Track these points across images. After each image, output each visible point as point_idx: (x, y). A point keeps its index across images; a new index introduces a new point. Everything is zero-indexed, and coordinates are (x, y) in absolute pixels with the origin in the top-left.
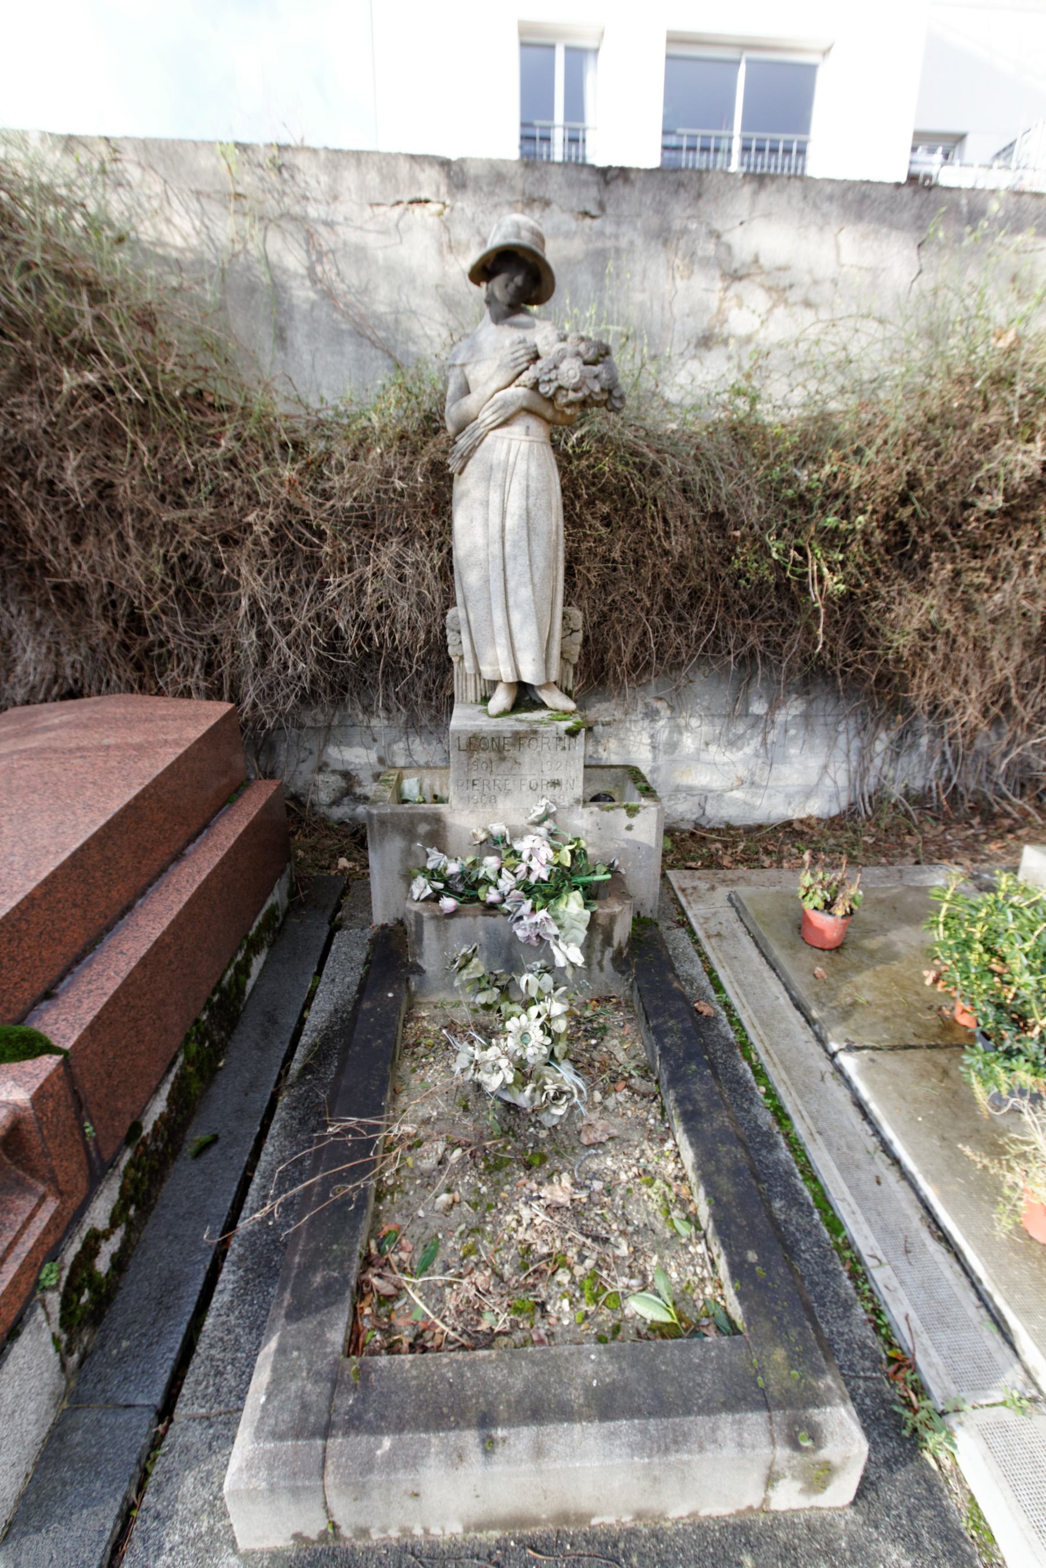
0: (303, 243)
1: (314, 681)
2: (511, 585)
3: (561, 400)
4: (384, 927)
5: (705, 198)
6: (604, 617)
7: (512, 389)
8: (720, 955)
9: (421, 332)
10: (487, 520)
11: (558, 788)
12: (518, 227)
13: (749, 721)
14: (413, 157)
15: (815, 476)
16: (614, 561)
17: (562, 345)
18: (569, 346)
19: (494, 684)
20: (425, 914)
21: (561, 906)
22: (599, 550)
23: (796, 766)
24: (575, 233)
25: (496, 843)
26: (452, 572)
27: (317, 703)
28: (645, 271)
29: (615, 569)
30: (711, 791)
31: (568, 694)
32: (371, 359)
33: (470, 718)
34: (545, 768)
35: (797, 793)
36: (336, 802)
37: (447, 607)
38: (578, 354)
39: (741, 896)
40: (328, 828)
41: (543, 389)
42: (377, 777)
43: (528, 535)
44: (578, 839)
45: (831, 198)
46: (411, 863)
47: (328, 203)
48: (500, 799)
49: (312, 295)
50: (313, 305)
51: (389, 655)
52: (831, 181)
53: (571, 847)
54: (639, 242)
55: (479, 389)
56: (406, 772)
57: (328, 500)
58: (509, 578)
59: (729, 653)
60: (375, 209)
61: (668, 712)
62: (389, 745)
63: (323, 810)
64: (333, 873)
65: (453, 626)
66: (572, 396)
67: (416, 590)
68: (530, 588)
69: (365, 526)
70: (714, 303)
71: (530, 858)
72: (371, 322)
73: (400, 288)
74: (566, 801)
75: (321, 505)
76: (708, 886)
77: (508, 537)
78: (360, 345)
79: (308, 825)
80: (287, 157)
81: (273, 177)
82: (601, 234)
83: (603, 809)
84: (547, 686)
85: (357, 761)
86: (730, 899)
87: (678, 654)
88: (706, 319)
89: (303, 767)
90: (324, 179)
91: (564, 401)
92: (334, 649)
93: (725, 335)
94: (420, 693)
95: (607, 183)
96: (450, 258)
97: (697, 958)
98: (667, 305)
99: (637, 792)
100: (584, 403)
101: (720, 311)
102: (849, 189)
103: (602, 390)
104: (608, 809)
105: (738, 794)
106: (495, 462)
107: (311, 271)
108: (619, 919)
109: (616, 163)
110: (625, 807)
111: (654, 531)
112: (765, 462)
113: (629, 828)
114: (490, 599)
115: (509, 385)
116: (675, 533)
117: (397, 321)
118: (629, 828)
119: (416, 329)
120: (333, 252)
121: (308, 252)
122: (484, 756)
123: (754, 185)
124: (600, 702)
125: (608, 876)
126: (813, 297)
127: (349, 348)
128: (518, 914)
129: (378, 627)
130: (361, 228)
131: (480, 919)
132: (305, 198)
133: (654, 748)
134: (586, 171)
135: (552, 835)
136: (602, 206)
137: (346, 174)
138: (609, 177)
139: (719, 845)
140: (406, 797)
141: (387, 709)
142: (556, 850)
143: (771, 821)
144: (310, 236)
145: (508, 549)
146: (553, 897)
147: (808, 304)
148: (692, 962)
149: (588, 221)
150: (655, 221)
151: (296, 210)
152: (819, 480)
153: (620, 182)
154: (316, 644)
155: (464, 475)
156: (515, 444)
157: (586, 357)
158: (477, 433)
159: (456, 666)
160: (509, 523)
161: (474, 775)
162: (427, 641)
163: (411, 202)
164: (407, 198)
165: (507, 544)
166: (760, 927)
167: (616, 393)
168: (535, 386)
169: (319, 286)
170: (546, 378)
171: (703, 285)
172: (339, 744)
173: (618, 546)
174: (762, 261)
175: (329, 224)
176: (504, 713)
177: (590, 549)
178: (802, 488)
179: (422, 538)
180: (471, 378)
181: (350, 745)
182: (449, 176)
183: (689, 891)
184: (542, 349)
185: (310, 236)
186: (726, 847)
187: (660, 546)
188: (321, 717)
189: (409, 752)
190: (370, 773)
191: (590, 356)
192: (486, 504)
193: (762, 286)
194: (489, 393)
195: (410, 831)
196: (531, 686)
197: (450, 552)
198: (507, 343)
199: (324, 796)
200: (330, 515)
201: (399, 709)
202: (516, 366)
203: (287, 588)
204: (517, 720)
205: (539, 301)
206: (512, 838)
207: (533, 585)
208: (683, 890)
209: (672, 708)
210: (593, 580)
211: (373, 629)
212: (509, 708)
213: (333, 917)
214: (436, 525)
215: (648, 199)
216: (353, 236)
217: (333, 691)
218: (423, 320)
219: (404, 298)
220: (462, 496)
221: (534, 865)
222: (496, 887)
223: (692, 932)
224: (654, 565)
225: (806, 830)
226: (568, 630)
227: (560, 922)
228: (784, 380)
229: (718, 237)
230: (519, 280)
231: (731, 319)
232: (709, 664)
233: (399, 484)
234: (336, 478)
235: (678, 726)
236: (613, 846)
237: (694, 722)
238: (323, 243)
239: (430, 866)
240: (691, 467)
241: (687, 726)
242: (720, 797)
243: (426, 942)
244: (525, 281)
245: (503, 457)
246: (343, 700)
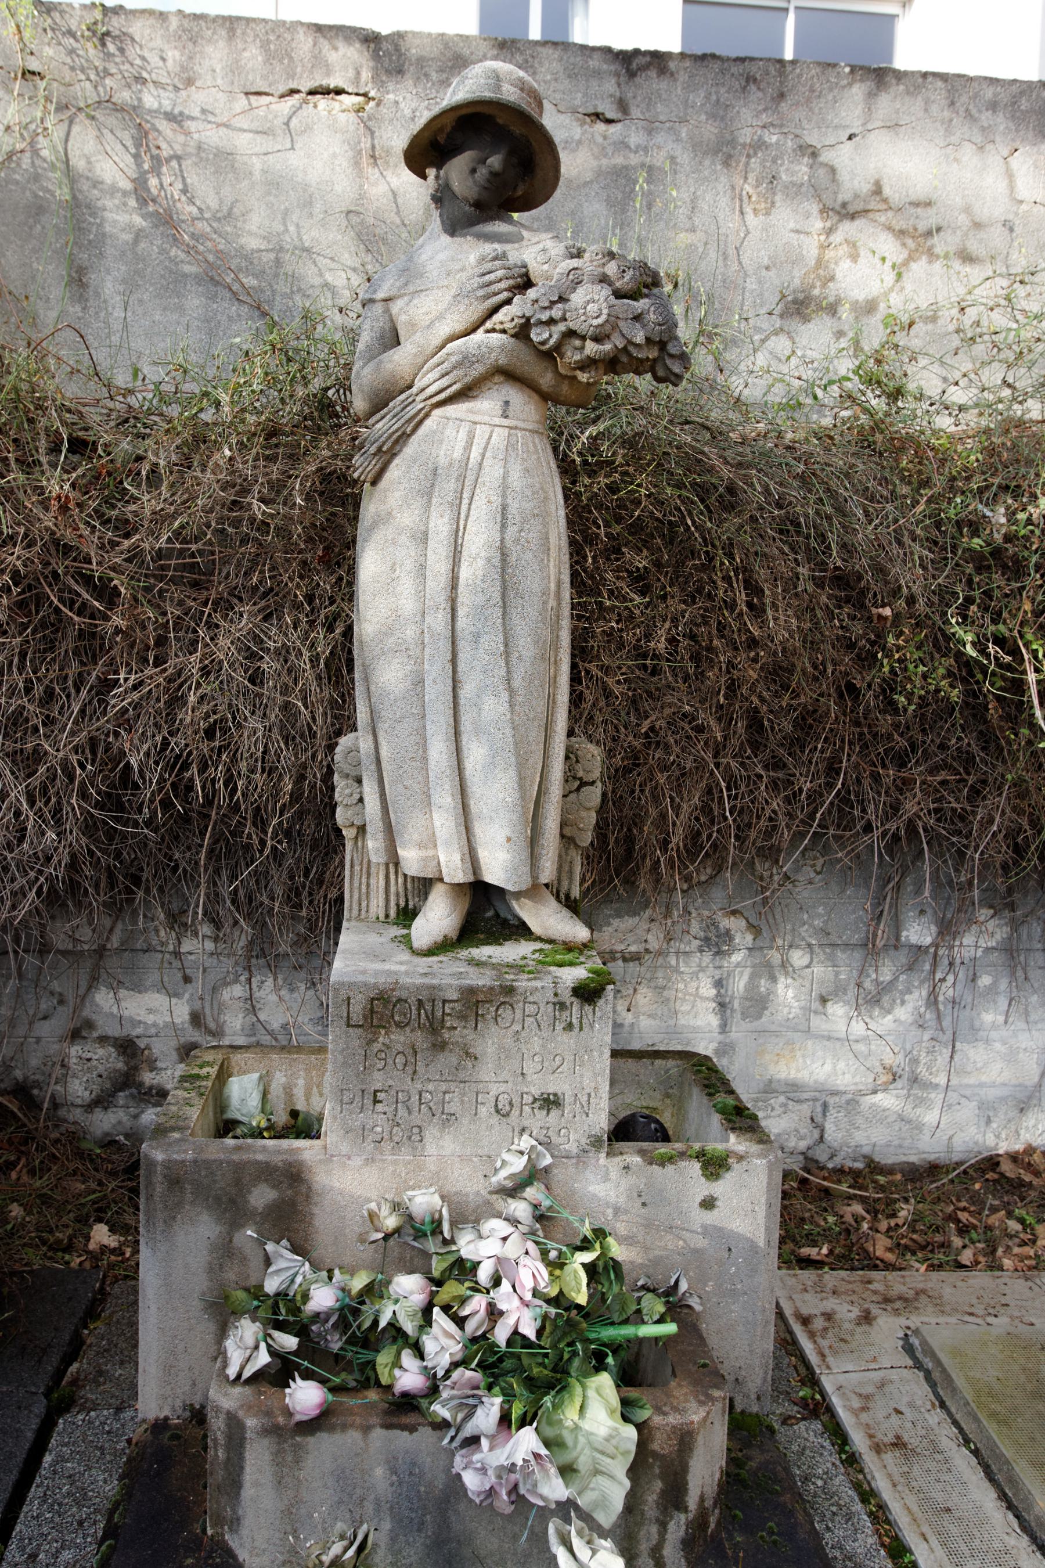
0: (129, 143)
1: (74, 865)
2: (467, 691)
3: (572, 356)
4: (160, 1426)
5: (790, 99)
6: (635, 759)
7: (479, 335)
8: (911, 1501)
9: (317, 281)
10: (423, 567)
11: (555, 1113)
12: (497, 77)
13: (903, 957)
14: (319, 28)
15: (1022, 516)
16: (655, 657)
17: (575, 263)
18: (587, 264)
19: (424, 886)
20: (251, 1423)
21: (570, 1415)
22: (628, 637)
23: (998, 1046)
24: (579, 142)
25: (420, 1235)
26: (351, 670)
27: (79, 905)
28: (694, 200)
29: (655, 671)
30: (834, 1093)
31: (572, 906)
32: (230, 319)
33: (374, 955)
34: (530, 1067)
35: (1003, 1099)
36: (102, 1101)
37: (339, 733)
38: (604, 279)
39: (934, 1344)
40: (80, 1155)
41: (537, 335)
42: (186, 1051)
43: (503, 597)
44: (600, 1233)
45: (993, 106)
46: (231, 1275)
47: (177, 89)
48: (431, 1134)
49: (138, 221)
50: (139, 235)
51: (224, 819)
52: (993, 81)
53: (588, 1257)
54: (684, 158)
55: (418, 337)
56: (237, 1058)
57: (127, 536)
58: (461, 675)
59: (868, 828)
60: (253, 98)
61: (749, 938)
62: (214, 989)
63: (77, 1115)
64: (76, 1261)
65: (347, 769)
66: (591, 348)
67: (280, 699)
68: (505, 695)
69: (195, 585)
70: (810, 248)
71: (497, 1282)
72: (234, 263)
73: (286, 213)
74: (572, 1141)
75: (114, 544)
76: (856, 1312)
77: (464, 599)
78: (213, 298)
79: (41, 1148)
80: (116, 24)
81: (91, 51)
82: (622, 145)
83: (651, 1160)
84: (533, 891)
85: (150, 1019)
86: (909, 1349)
87: (771, 831)
88: (798, 274)
89: (45, 1029)
90: (173, 55)
91: (577, 357)
92: (120, 807)
93: (831, 299)
94: (279, 891)
95: (632, 75)
96: (373, 173)
97: (858, 1507)
98: (731, 252)
99: (716, 1119)
100: (613, 364)
101: (819, 262)
102: (1022, 93)
103: (648, 340)
104: (664, 1161)
105: (888, 1101)
106: (443, 461)
107: (140, 184)
108: (700, 1440)
109: (647, 45)
110: (700, 1155)
111: (732, 606)
112: (927, 492)
113: (708, 1204)
114: (424, 717)
115: (474, 330)
116: (775, 607)
117: (278, 262)
118: (708, 1204)
119: (310, 275)
120: (178, 158)
121: (136, 156)
122: (399, 1039)
123: (869, 85)
124: (619, 915)
125: (670, 1328)
126: (974, 247)
127: (194, 302)
128: (468, 1431)
129: (203, 768)
130: (226, 126)
131: (378, 1434)
132: (140, 80)
133: (722, 1005)
134: (596, 55)
135: (541, 1217)
136: (623, 106)
137: (209, 49)
138: (634, 66)
139: (858, 1208)
140: (233, 1114)
141: (216, 923)
142: (556, 1265)
143: (956, 1158)
144: (142, 135)
145: (462, 622)
146: (549, 1386)
147: (967, 258)
148: (849, 1517)
149: (601, 127)
150: (710, 131)
151: (124, 96)
152: (1029, 521)
153: (653, 73)
154: (84, 795)
155: (383, 484)
156: (481, 432)
157: (618, 284)
158: (412, 410)
159: (349, 846)
160: (465, 573)
161: (378, 1080)
162: (296, 796)
163: (311, 93)
164: (305, 86)
165: (461, 612)
166: (992, 1428)
167: (672, 349)
168: (522, 332)
169: (151, 208)
170: (544, 316)
171: (792, 225)
172: (116, 985)
173: (662, 633)
174: (887, 191)
175: (176, 119)
176: (442, 947)
177: (609, 634)
178: (998, 537)
179: (297, 606)
180: (402, 320)
181: (138, 987)
182: (376, 57)
183: (819, 1323)
184: (536, 269)
185: (142, 135)
186: (874, 1213)
187: (744, 629)
188: (85, 933)
189: (251, 1005)
190: (174, 1043)
191: (624, 283)
192: (423, 538)
193: (889, 229)
194: (436, 342)
195: (233, 1201)
196: (500, 891)
197: (348, 632)
198: (472, 258)
199: (79, 1089)
200: (129, 560)
201: (236, 923)
202: (488, 297)
203: (38, 690)
204: (474, 963)
205: (527, 204)
206: (453, 1224)
207: (511, 691)
208: (805, 1321)
209: (755, 929)
210: (617, 690)
211: (194, 769)
212: (454, 935)
213: (60, 1373)
214: (325, 584)
215: (698, 98)
216: (212, 136)
217: (112, 884)
218: (322, 262)
219: (292, 229)
220: (375, 525)
221: (504, 1297)
222: (420, 1355)
223: (838, 1435)
224: (731, 665)
225: (1027, 1178)
226: (574, 782)
227: (566, 1458)
228: (936, 368)
229: (814, 155)
230: (495, 161)
231: (839, 276)
232: (826, 850)
233: (258, 509)
234: (147, 497)
235: (768, 965)
236: (670, 1243)
237: (798, 958)
238: (164, 146)
239: (272, 1285)
240: (795, 493)
241: (784, 964)
242: (852, 1104)
243: (248, 1492)
244: (506, 162)
245: (457, 454)
246: (130, 901)
